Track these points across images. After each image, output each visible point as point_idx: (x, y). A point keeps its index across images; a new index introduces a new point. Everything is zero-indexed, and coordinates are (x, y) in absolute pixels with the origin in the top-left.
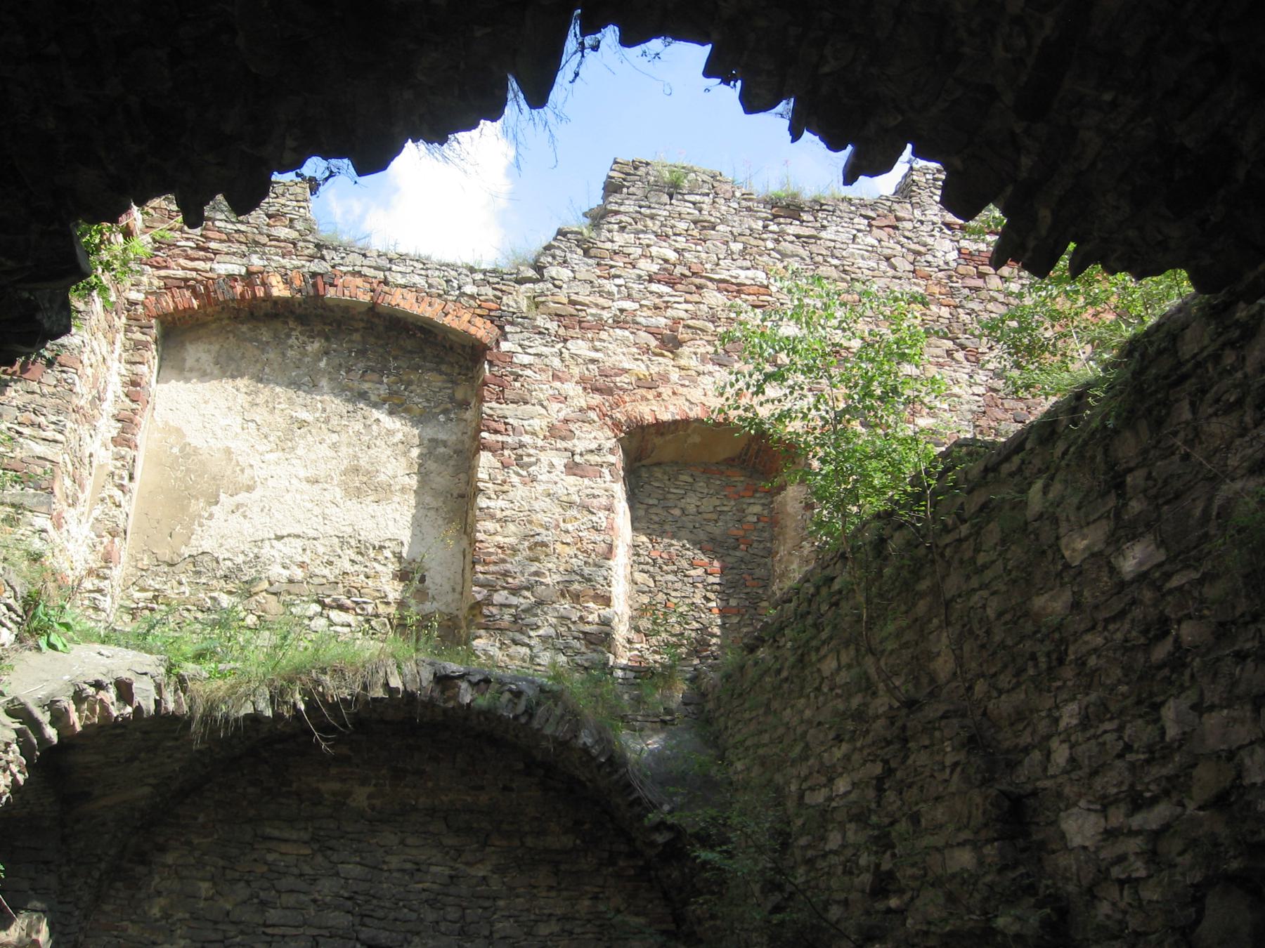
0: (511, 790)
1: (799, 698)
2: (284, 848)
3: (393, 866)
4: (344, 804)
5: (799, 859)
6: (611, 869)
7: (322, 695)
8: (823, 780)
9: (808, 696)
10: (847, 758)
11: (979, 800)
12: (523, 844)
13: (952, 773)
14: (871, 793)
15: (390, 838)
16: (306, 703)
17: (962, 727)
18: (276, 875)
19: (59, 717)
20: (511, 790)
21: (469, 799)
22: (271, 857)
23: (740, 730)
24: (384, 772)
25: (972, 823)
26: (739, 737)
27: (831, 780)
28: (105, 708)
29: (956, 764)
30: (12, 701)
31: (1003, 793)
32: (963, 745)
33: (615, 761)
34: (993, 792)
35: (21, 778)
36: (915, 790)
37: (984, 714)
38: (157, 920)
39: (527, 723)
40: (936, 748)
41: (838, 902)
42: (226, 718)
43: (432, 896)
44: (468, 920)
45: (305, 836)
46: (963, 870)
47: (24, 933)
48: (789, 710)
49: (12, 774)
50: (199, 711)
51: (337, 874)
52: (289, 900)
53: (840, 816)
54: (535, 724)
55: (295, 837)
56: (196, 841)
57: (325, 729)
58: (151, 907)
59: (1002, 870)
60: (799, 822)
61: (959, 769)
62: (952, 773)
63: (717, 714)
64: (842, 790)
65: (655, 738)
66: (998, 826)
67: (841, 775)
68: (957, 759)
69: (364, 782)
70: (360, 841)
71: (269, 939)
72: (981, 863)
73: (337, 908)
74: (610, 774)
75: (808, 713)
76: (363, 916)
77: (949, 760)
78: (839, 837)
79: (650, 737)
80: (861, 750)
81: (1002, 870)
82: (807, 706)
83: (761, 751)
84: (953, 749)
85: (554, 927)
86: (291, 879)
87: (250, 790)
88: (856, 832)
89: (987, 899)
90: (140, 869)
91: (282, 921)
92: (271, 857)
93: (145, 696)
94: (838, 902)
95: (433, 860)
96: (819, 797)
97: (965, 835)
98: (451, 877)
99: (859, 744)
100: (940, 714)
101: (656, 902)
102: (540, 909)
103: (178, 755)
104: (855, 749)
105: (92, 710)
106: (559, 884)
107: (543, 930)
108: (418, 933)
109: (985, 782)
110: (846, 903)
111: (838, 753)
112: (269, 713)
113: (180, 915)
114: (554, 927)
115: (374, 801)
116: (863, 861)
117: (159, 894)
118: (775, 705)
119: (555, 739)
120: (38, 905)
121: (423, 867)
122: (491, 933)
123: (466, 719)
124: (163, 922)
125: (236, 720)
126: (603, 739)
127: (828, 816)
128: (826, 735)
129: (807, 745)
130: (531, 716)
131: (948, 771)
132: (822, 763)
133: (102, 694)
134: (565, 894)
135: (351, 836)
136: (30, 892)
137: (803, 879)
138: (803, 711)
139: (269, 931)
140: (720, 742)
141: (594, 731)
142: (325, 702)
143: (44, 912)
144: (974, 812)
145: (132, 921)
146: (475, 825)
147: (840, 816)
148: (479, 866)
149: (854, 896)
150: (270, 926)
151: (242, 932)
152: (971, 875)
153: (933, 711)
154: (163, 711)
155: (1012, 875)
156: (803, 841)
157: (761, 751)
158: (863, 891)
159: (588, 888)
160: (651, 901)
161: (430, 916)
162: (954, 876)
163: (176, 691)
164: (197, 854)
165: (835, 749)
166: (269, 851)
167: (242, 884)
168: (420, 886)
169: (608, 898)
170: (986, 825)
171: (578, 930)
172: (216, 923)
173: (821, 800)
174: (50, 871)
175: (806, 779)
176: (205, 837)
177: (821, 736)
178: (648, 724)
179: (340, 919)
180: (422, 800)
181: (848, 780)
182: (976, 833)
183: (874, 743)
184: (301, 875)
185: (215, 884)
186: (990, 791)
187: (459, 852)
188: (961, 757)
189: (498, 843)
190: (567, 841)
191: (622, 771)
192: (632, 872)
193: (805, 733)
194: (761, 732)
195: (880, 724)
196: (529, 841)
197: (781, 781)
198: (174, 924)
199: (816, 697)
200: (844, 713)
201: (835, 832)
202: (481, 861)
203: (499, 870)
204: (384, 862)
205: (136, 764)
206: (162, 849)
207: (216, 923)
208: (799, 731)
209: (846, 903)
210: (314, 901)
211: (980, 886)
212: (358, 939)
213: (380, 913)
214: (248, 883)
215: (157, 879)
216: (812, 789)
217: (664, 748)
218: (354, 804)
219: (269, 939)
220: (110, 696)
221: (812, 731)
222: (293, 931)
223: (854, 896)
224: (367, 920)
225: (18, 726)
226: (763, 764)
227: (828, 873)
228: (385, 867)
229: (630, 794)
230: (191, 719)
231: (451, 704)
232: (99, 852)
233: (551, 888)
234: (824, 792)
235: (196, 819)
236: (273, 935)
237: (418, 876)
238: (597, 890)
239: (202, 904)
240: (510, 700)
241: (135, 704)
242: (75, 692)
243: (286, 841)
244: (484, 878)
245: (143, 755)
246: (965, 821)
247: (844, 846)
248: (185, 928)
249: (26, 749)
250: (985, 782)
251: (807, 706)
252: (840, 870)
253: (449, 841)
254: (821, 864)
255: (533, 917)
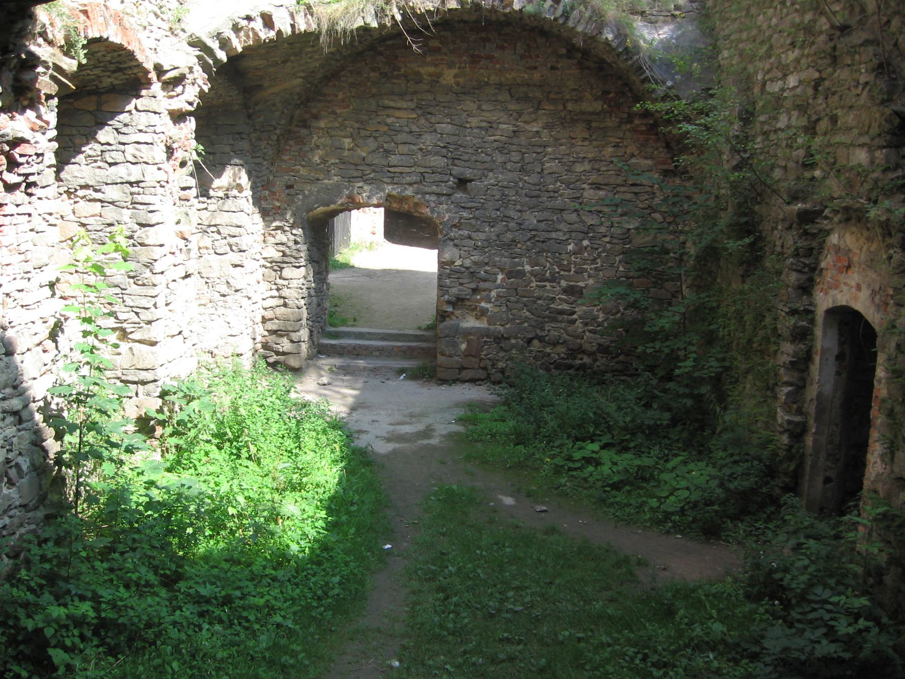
0: (558, 69)
1: (769, 8)
2: (398, 114)
3: (473, 125)
4: (438, 82)
5: (758, 130)
6: (628, 126)
7: (413, 8)
8: (780, 75)
9: (776, 8)
10: (797, 61)
11: (877, 115)
12: (565, 108)
13: (863, 89)
14: (810, 92)
15: (471, 105)
16: (402, 15)
17: (875, 55)
18: (394, 133)
19: (225, 44)
20: (558, 69)
21: (526, 76)
22: (389, 121)
23: (728, 26)
24: (465, 58)
25: (871, 132)
26: (727, 32)
27: (785, 76)
28: (256, 34)
29: (867, 83)
30: (191, 36)
31: (896, 113)
32: (873, 70)
33: (630, 52)
34: (888, 111)
35: (206, 89)
36: (836, 98)
37: (896, 45)
38: (318, 165)
39: (564, 23)
40: (855, 68)
41: (781, 167)
42: (345, 31)
43: (501, 145)
44: (526, 161)
45: (412, 105)
46: (860, 165)
47: (231, 180)
48: (761, 17)
49: (199, 86)
50: (325, 28)
51: (435, 131)
52: (404, 149)
53: (788, 104)
54: (570, 24)
55: (405, 106)
56: (339, 111)
57: (413, 32)
58: (313, 156)
59: (886, 170)
60: (761, 104)
61: (868, 88)
62: (863, 89)
63: (714, 11)
64: (792, 85)
65: (666, 29)
66: (888, 137)
67: (792, 73)
68: (868, 79)
69: (451, 66)
70: (449, 108)
71: (392, 175)
72: (872, 162)
73: (436, 154)
74: (626, 60)
75: (774, 21)
76: (454, 159)
77: (862, 80)
78: (786, 120)
79: (661, 28)
80: (808, 56)
81: (886, 170)
82: (774, 15)
83: (741, 46)
84: (866, 71)
85: (587, 166)
86: (404, 135)
87: (372, 74)
88: (798, 118)
89: (872, 190)
90: (304, 131)
91: (400, 163)
92: (389, 121)
93: (283, 24)
94: (781, 167)
95: (502, 120)
96: (774, 88)
97: (865, 139)
98: (514, 132)
99: (806, 52)
100: (860, 42)
101: (661, 150)
102: (577, 153)
103: (317, 57)
104: (803, 55)
105: (248, 36)
106: (591, 136)
107: (579, 168)
108: (492, 170)
109: (883, 102)
110: (785, 168)
111: (792, 56)
112: (375, 24)
113: (333, 161)
114: (587, 166)
115: (458, 79)
116: (800, 140)
117: (318, 147)
118: (753, 11)
119: (585, 34)
120: (238, 161)
121: (495, 125)
122: (542, 170)
123: (521, 19)
124: (322, 166)
125: (352, 31)
126: (621, 36)
127: (781, 102)
128: (785, 40)
129: (771, 47)
130: (567, 18)
131: (860, 87)
132: (780, 62)
133: (252, 24)
134: (595, 143)
135: (442, 104)
136: (232, 153)
137: (760, 146)
138: (771, 19)
139: (390, 169)
140: (714, 33)
141: (615, 29)
142: (415, 14)
143: (242, 165)
144: (873, 124)
145: (302, 166)
146: (530, 95)
147: (788, 104)
148: (534, 124)
149: (791, 164)
150: (391, 167)
151: (374, 171)
152: (864, 171)
153: (857, 38)
154: (297, 32)
155: (892, 175)
156: (762, 118)
157: (741, 46)
158: (797, 163)
159: (612, 139)
160: (657, 149)
161: (500, 158)
162: (852, 169)
163: (306, 15)
164: (340, 120)
165: (790, 53)
166: (388, 116)
167: (371, 139)
168: (493, 138)
169: (626, 147)
170: (879, 135)
171: (604, 169)
172: (356, 165)
173: (777, 90)
174: (243, 139)
175: (768, 72)
176: (344, 108)
177: (782, 40)
178: (661, 18)
179: (438, 161)
180: (492, 77)
181: (797, 77)
182: (872, 139)
183: (815, 54)
184: (411, 132)
185: (354, 139)
186: (886, 109)
187: (520, 114)
188: (871, 78)
189: (547, 108)
190: (598, 106)
191: (636, 57)
192: (644, 128)
193: (771, 37)
194: (741, 31)
195: (823, 38)
196: (570, 106)
197: (752, 71)
198: (329, 167)
199: (781, 10)
200: (799, 25)
201: (784, 115)
202: (535, 120)
203: (548, 126)
204: (467, 122)
205: (289, 64)
206: (316, 117)
207: (356, 165)
208: (767, 34)
209: (785, 168)
210: (421, 149)
211: (869, 179)
212: (451, 174)
213: (466, 157)
214: (375, 138)
215: (315, 138)
216: (772, 80)
217: (672, 38)
218: (444, 82)
219: (392, 175)
220: (258, 25)
221: (775, 36)
222: (408, 170)
223: (791, 164)
224: (456, 162)
225: (198, 53)
226: (741, 55)
227: (776, 144)
228: (468, 126)
229: (641, 75)
230: (320, 33)
231: (508, 10)
232: (274, 123)
233: (585, 139)
234: (780, 83)
235: (337, 96)
236: (394, 173)
237: (491, 131)
238: (618, 140)
239: (346, 153)
240: (551, 6)
241: (276, 29)
242: (233, 25)
243: (399, 109)
244: (537, 132)
245: (292, 58)
246: (866, 129)
247: (789, 127)
248: (336, 169)
249: (205, 68)
250: (883, 102)
251: (774, 15)
252: (784, 143)
253: (512, 107)
254: (773, 137)
255: (572, 159)
